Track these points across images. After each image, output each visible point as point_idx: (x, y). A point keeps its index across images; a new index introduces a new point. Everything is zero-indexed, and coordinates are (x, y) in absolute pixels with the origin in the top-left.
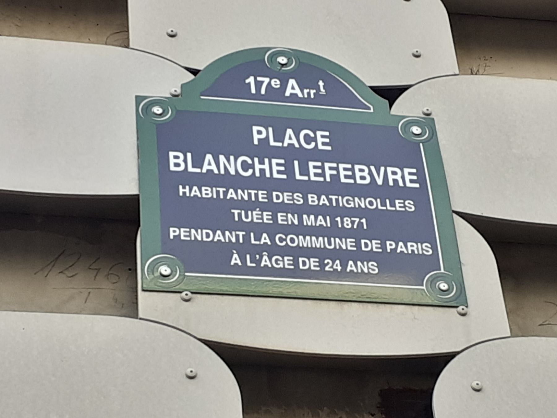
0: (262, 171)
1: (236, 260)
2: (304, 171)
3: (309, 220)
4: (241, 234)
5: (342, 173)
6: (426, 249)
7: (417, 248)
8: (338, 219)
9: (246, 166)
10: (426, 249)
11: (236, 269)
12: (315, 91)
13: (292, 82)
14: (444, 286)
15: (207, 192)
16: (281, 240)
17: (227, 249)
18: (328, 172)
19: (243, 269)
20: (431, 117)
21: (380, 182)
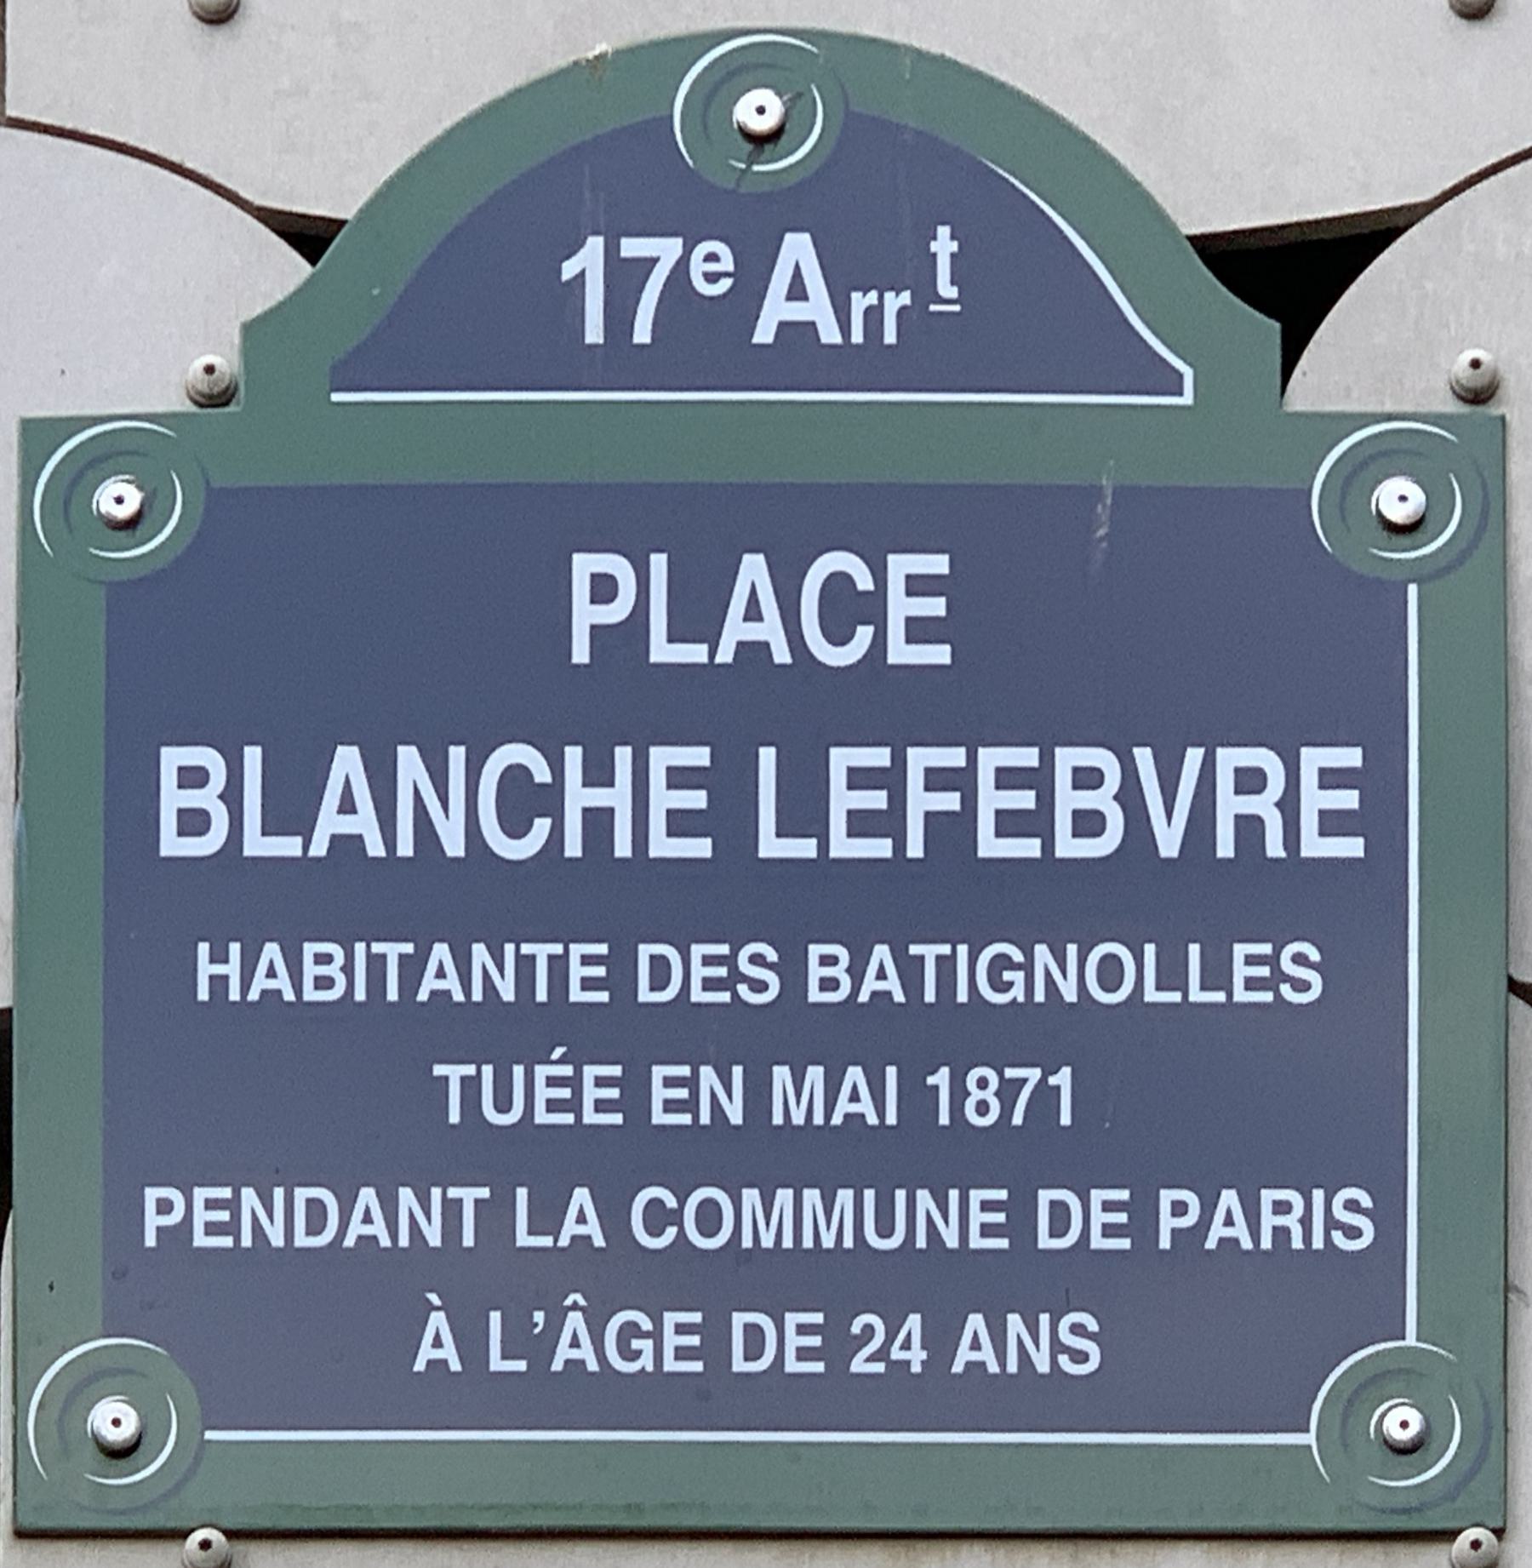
0: (598, 822)
1: (437, 1345)
2: (804, 810)
3: (797, 1096)
4: (469, 1196)
5: (991, 800)
6: (1340, 1218)
7: (1306, 1222)
8: (941, 1079)
9: (524, 801)
10: (1340, 1218)
11: (445, 1398)
12: (905, 298)
13: (798, 249)
14: (1400, 1421)
15: (328, 972)
16: (658, 1218)
17: (386, 1285)
18: (920, 802)
19: (467, 1395)
20: (1493, 410)
21: (1169, 840)
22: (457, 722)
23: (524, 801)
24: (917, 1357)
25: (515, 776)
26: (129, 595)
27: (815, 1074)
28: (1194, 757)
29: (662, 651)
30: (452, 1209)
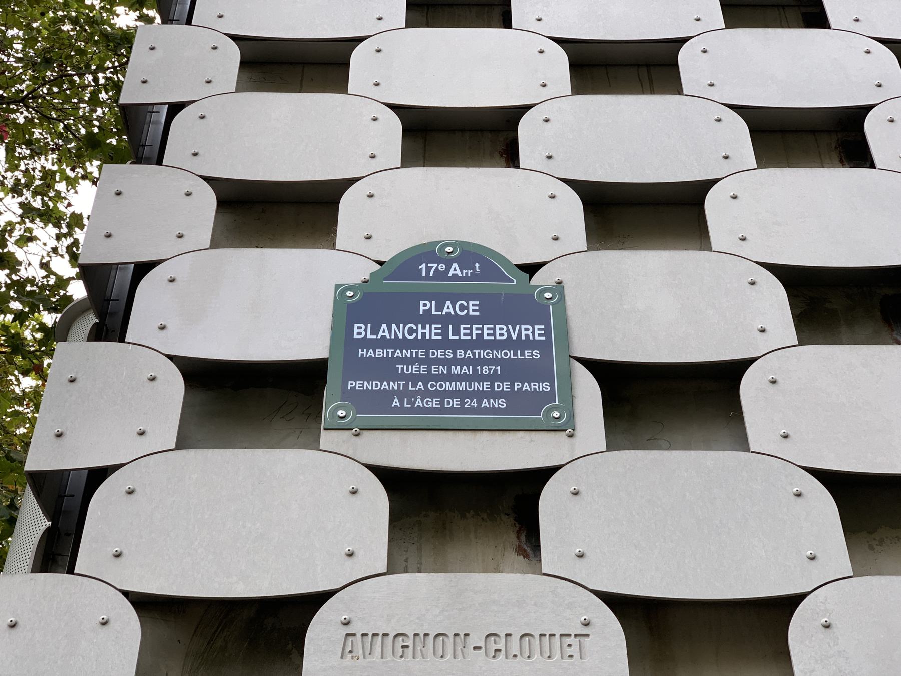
0: (424, 334)
1: (396, 402)
3: (456, 370)
4: (402, 383)
6: (546, 386)
8: (479, 367)
10: (546, 386)
11: (396, 410)
13: (455, 265)
14: (556, 414)
15: (380, 353)
16: (432, 386)
18: (474, 332)
19: (401, 410)
21: (514, 337)
22: (401, 321)
24: (475, 405)
25: (411, 328)
26: (350, 306)
27: (458, 367)
28: (518, 327)
29: (434, 313)
30: (399, 385)
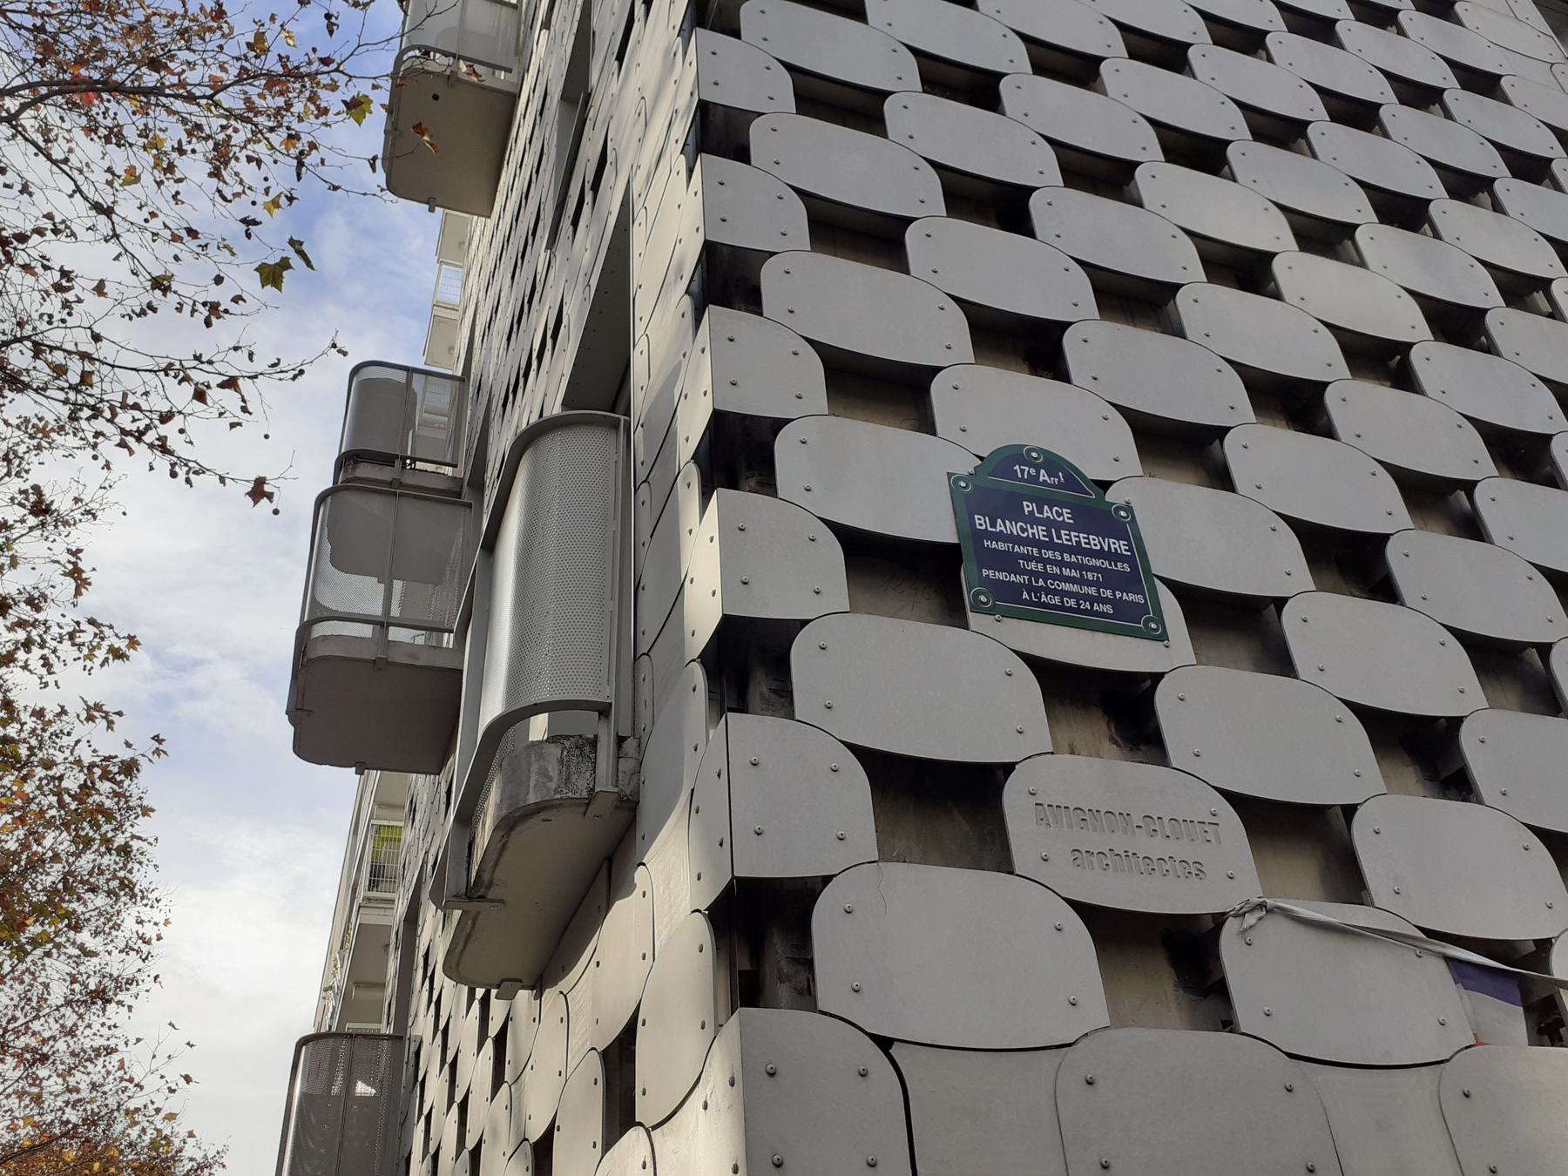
3: (1066, 572)
10: (1139, 598)
11: (1025, 602)
15: (1002, 546)
17: (1018, 588)
23: (1024, 531)
